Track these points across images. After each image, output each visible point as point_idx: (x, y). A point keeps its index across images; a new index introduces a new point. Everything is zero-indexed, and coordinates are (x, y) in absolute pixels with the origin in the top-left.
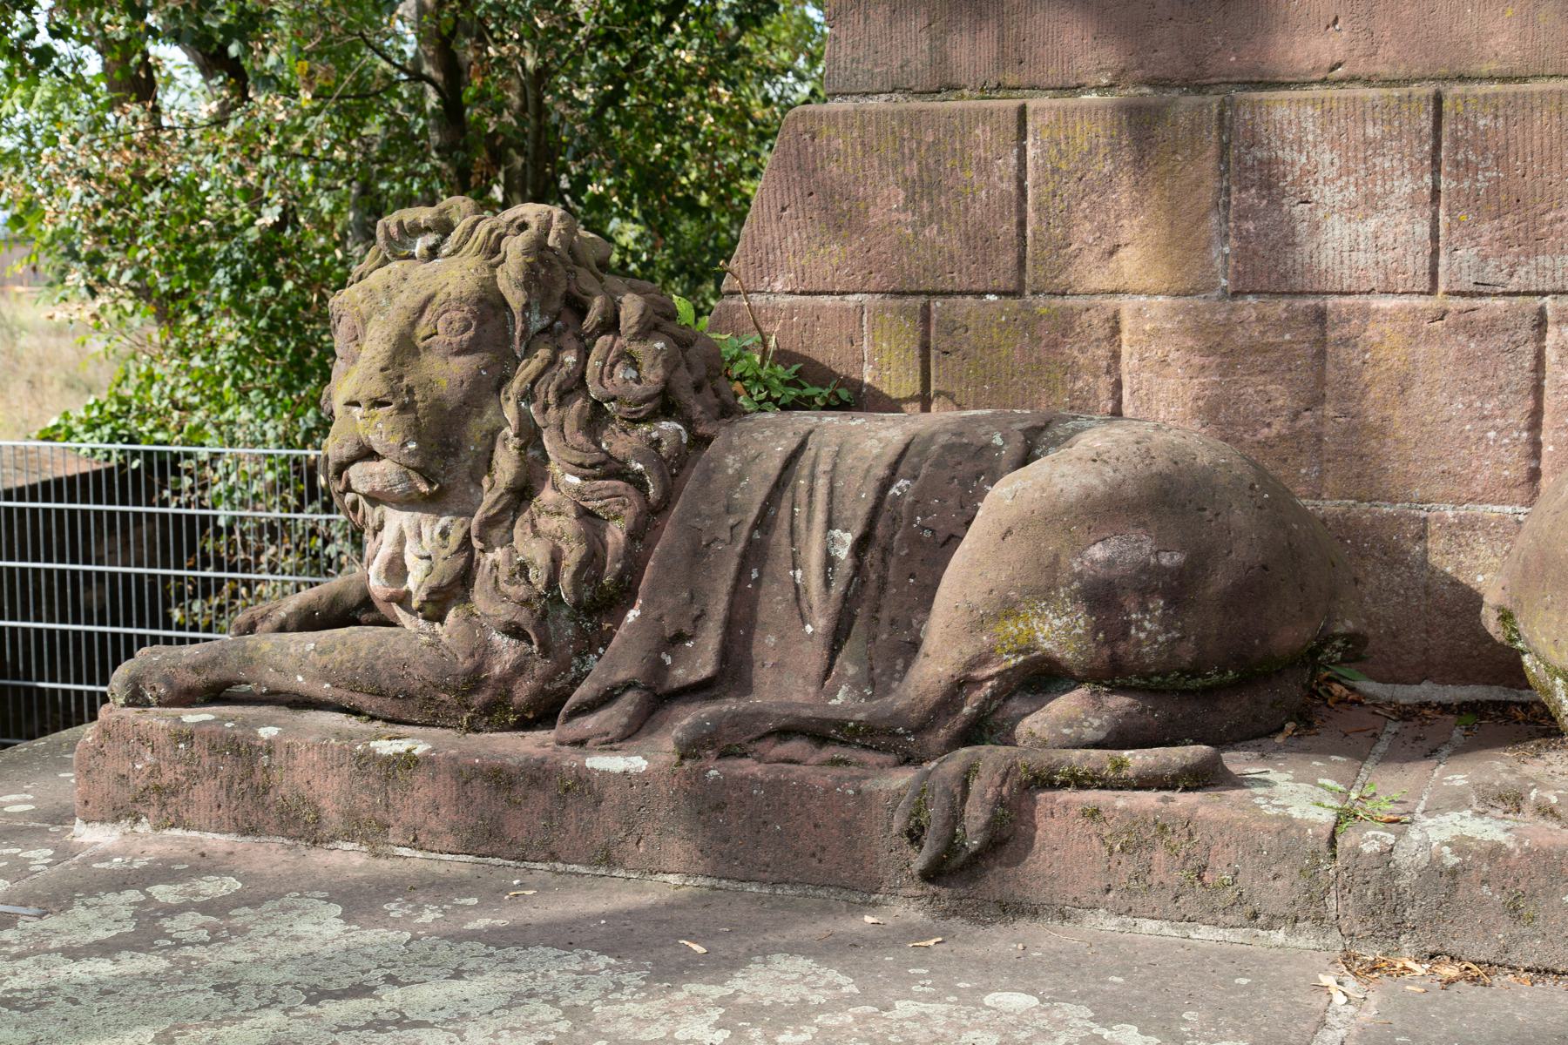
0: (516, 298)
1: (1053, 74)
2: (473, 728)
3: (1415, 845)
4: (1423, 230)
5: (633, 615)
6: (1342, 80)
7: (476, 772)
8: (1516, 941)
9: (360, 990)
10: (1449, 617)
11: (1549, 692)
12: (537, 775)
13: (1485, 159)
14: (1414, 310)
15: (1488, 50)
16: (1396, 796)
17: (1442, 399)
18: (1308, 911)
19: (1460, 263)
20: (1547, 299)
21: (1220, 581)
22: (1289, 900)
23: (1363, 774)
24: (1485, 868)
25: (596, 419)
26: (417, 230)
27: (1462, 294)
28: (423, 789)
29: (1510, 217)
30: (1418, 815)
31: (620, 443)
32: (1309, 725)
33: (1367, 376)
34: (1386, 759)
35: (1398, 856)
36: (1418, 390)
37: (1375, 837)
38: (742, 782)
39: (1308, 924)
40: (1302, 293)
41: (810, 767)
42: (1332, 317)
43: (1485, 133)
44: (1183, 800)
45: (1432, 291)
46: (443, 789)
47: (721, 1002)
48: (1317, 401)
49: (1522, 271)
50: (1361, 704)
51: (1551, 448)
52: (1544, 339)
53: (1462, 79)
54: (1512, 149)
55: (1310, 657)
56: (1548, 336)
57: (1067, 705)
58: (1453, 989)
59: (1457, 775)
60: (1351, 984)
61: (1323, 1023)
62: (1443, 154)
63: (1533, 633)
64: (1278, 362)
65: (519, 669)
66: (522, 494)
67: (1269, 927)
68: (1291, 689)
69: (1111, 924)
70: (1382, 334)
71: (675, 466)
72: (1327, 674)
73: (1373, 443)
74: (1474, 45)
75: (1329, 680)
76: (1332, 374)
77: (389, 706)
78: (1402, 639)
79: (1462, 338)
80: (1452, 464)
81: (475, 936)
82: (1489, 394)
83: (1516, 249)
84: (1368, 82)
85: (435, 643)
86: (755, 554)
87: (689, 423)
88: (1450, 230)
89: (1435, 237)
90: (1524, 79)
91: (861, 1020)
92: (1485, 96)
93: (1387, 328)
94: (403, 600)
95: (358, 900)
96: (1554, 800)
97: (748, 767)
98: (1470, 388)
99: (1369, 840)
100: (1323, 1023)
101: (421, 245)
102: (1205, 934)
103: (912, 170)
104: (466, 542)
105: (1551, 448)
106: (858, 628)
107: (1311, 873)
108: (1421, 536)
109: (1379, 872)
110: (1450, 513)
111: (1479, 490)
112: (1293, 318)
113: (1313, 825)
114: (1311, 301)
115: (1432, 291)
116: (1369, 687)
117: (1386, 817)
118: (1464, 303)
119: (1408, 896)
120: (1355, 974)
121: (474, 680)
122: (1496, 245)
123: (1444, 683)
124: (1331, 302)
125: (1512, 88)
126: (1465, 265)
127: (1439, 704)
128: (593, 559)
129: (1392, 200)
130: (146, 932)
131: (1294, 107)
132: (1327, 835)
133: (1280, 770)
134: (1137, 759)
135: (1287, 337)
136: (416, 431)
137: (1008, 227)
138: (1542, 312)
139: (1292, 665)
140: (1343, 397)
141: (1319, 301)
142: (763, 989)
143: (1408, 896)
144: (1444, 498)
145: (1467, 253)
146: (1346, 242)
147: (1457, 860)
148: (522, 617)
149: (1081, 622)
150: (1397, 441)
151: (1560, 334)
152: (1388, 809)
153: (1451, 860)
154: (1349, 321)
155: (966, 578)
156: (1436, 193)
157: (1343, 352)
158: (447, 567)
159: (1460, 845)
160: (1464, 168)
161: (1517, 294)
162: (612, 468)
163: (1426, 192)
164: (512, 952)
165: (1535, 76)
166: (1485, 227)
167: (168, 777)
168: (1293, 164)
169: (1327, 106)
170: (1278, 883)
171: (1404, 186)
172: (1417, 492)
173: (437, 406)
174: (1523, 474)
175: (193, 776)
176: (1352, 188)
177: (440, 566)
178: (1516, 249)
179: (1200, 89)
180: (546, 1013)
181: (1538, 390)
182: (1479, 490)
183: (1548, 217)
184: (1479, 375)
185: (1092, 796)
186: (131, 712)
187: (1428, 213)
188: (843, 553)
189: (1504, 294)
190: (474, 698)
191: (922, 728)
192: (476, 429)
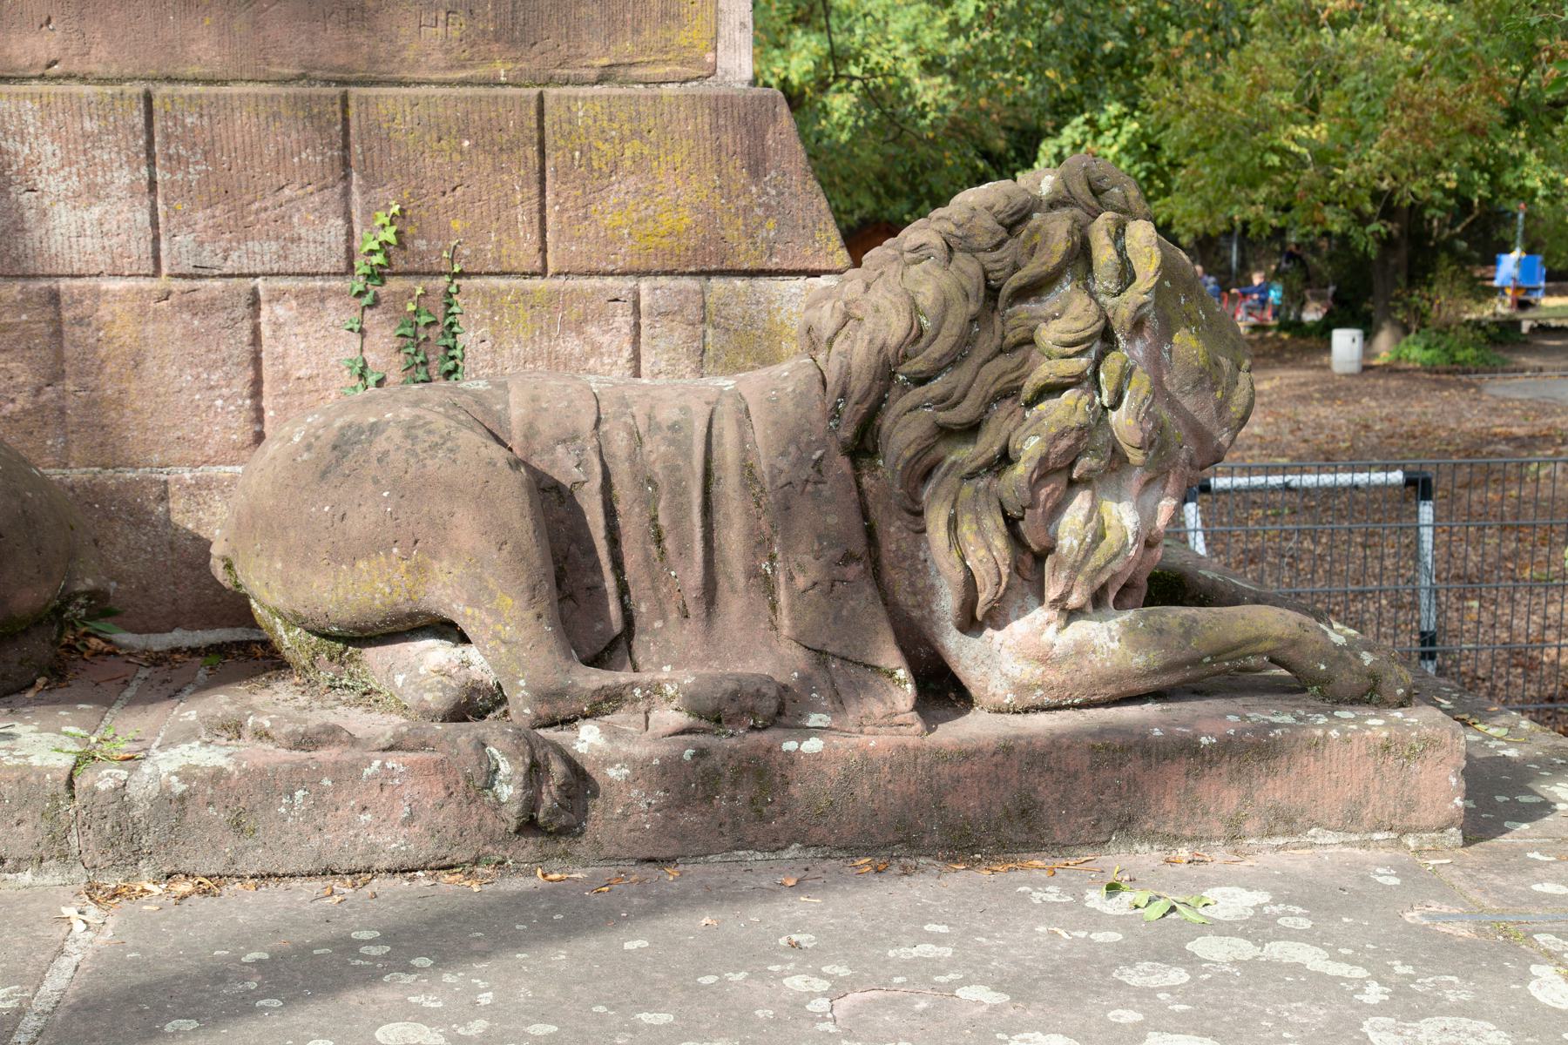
3: (146, 778)
4: (143, 217)
6: (59, 77)
8: (241, 852)
10: (194, 569)
11: (272, 629)
13: (195, 154)
14: (140, 291)
15: (191, 55)
16: (131, 735)
17: (172, 371)
18: (54, 850)
19: (179, 248)
20: (259, 280)
22: (33, 842)
23: (108, 719)
24: (209, 791)
27: (184, 276)
29: (220, 206)
30: (153, 749)
32: (62, 678)
33: (103, 352)
34: (132, 702)
35: (132, 790)
36: (150, 365)
37: (109, 775)
39: (53, 862)
40: (35, 276)
42: (65, 299)
43: (192, 130)
45: (156, 273)
48: (57, 376)
49: (234, 255)
50: (116, 654)
51: (272, 413)
52: (258, 316)
53: (170, 80)
54: (217, 145)
55: (55, 615)
56: (262, 313)
58: (186, 903)
59: (189, 712)
60: (93, 912)
61: (61, 952)
62: (157, 148)
63: (248, 578)
64: (17, 341)
67: (17, 870)
68: (39, 647)
70: (113, 313)
72: (84, 629)
73: (113, 414)
74: (179, 49)
75: (87, 635)
76: (69, 351)
78: (153, 592)
79: (186, 316)
80: (185, 431)
82: (213, 366)
83: (228, 236)
84: (83, 79)
88: (168, 217)
89: (155, 224)
90: (225, 82)
92: (190, 96)
93: (118, 308)
96: (267, 724)
98: (196, 361)
99: (104, 779)
100: (61, 952)
105: (272, 413)
107: (52, 815)
108: (163, 497)
109: (115, 806)
110: (187, 475)
111: (212, 453)
112: (28, 300)
113: (50, 770)
114: (44, 284)
115: (156, 273)
116: (125, 638)
117: (122, 755)
118: (185, 284)
119: (143, 825)
120: (97, 902)
122: (210, 232)
123: (193, 629)
124: (63, 284)
125: (214, 90)
126: (184, 250)
127: (189, 648)
129: (112, 189)
131: (13, 101)
132: (65, 778)
133: (27, 723)
135: (24, 317)
138: (255, 292)
139: (38, 623)
140: (81, 373)
141: (52, 283)
143: (143, 825)
144: (181, 462)
145: (184, 239)
146: (73, 227)
147: (184, 787)
150: (135, 411)
151: (272, 312)
152: (124, 748)
153: (179, 788)
154: (81, 302)
156: (152, 184)
157: (78, 331)
159: (185, 775)
160: (175, 161)
161: (232, 276)
163: (144, 183)
165: (235, 80)
166: (199, 215)
168: (16, 154)
169: (45, 101)
170: (22, 828)
171: (123, 177)
172: (156, 457)
174: (249, 437)
176: (75, 178)
178: (228, 236)
181: (257, 361)
182: (212, 453)
183: (254, 207)
184: (203, 349)
187: (147, 202)
189: (220, 276)
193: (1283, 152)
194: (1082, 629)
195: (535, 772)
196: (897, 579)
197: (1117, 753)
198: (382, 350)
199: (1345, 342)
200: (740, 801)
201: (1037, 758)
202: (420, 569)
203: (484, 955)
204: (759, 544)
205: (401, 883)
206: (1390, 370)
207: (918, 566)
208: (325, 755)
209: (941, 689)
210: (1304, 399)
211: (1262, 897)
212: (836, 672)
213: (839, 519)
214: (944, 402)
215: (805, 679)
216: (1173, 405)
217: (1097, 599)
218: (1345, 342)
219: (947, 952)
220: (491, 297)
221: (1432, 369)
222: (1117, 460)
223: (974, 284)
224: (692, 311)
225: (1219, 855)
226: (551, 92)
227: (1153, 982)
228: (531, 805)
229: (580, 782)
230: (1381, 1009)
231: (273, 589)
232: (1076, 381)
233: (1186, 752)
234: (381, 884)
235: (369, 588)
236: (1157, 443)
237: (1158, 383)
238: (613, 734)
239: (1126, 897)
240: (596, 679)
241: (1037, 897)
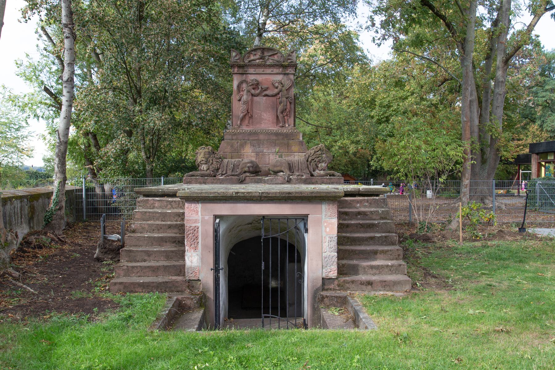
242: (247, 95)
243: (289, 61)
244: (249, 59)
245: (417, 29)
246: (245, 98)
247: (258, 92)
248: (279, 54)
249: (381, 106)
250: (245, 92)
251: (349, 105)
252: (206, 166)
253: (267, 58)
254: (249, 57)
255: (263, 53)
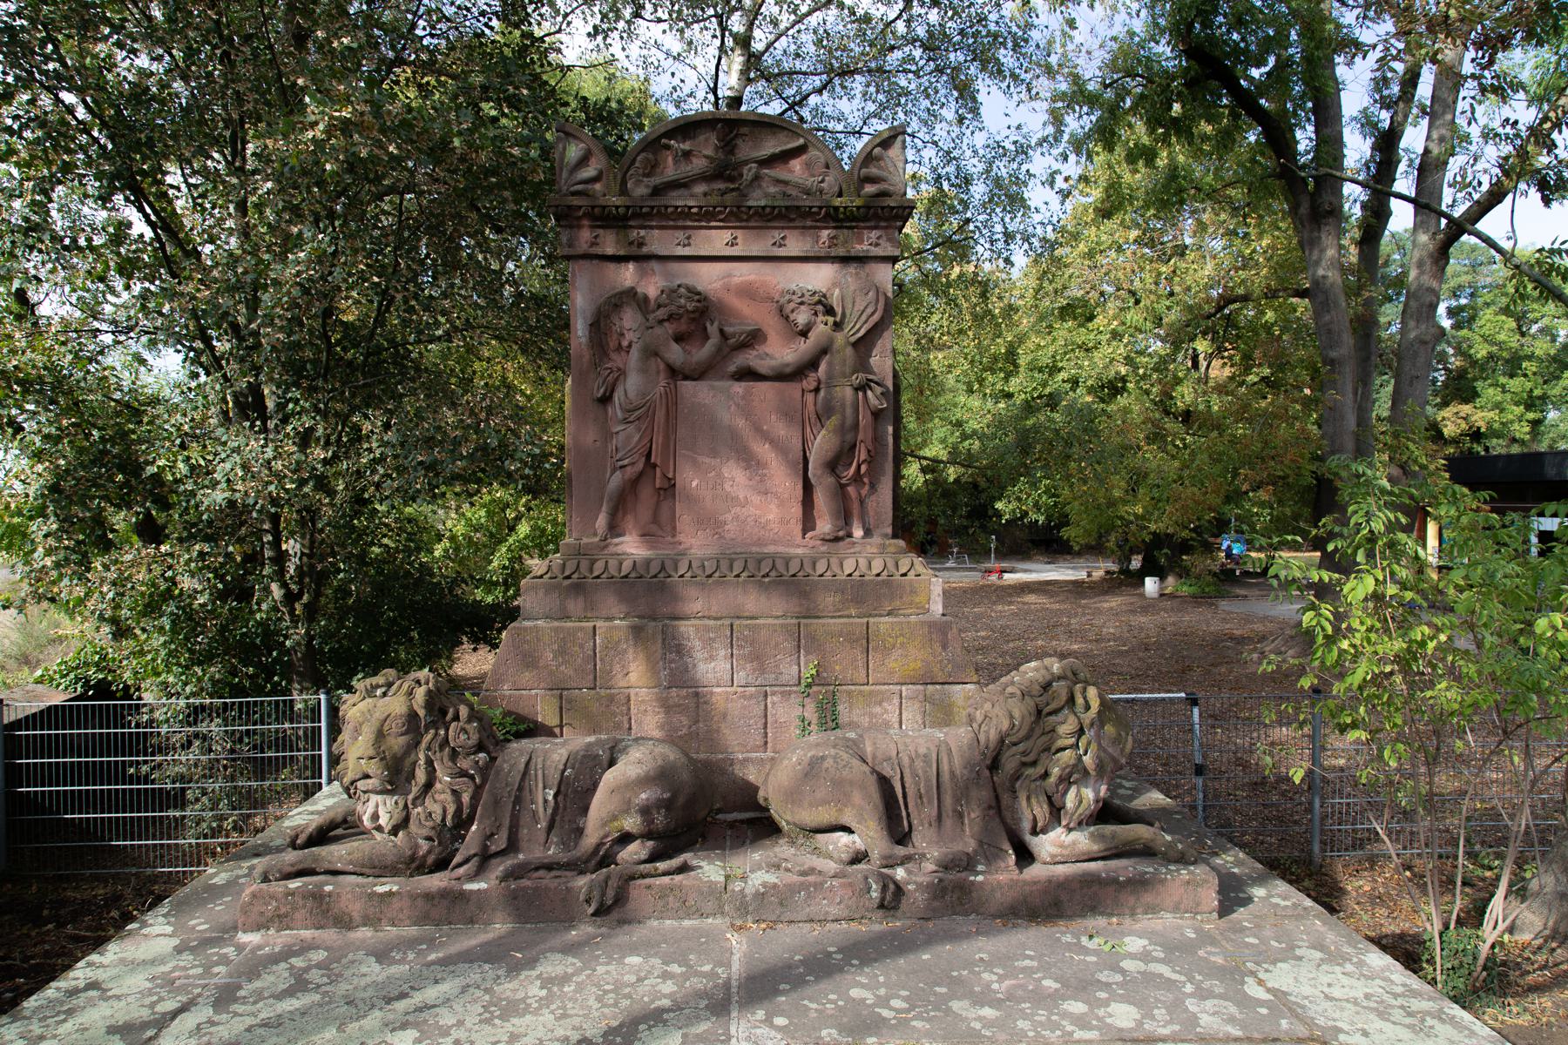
0: (422, 713)
1: (604, 613)
2: (411, 876)
5: (474, 828)
7: (418, 895)
9: (403, 996)
12: (444, 894)
19: (740, 677)
21: (681, 800)
25: (454, 755)
26: (378, 686)
28: (396, 903)
31: (464, 763)
38: (525, 889)
41: (547, 880)
44: (678, 878)
46: (406, 903)
47: (539, 977)
57: (633, 847)
65: (429, 852)
66: (429, 786)
69: (656, 923)
71: (485, 771)
77: (377, 871)
81: (433, 963)
85: (395, 846)
86: (518, 800)
87: (488, 753)
91: (588, 976)
94: (379, 829)
95: (382, 955)
97: (525, 882)
99: (737, 886)
101: (379, 692)
102: (686, 923)
103: (555, 647)
104: (406, 805)
106: (557, 824)
121: (413, 858)
128: (459, 810)
130: (300, 985)
134: (662, 866)
136: (387, 768)
137: (591, 666)
142: (549, 969)
148: (432, 833)
149: (639, 820)
155: (600, 805)
158: (398, 816)
159: (764, 885)
162: (463, 774)
164: (452, 968)
167: (283, 910)
171: (722, 653)
173: (394, 757)
175: (295, 909)
177: (396, 816)
179: (654, 619)
180: (478, 993)
185: (648, 881)
186: (264, 885)
188: (550, 798)
190: (415, 865)
191: (587, 861)
192: (408, 762)
193: (1121, 518)
194: (1075, 835)
195: (884, 888)
196: (1007, 815)
197: (1089, 882)
198: (811, 713)
199: (1151, 585)
200: (955, 900)
201: (1064, 885)
202: (840, 810)
203: (876, 960)
204: (957, 800)
205: (836, 926)
206: (1172, 596)
207: (1014, 811)
208: (811, 878)
209: (1025, 856)
210: (1133, 612)
211: (1145, 942)
212: (988, 852)
213: (985, 794)
214: (1024, 753)
215: (975, 851)
216: (1105, 751)
217: (1080, 824)
218: (1151, 585)
219: (1035, 964)
220: (849, 693)
221: (1194, 596)
222: (1086, 772)
223: (1033, 710)
224: (921, 697)
225: (1127, 921)
226: (871, 620)
227: (1110, 980)
228: (883, 899)
229: (899, 890)
230: (1191, 995)
231: (782, 813)
232: (1071, 747)
233: (1112, 882)
234: (829, 926)
235: (824, 816)
236: (1100, 767)
237: (1099, 744)
238: (909, 872)
239: (1096, 940)
240: (901, 851)
241: (1064, 939)
242: (643, 371)
243: (870, 189)
244: (656, 180)
245: (1177, 154)
246: (632, 386)
247: (703, 352)
248: (813, 152)
249: (1033, 367)
250: (635, 353)
251: (950, 366)
252: (390, 801)
253: (748, 172)
254: (652, 168)
255: (728, 146)
